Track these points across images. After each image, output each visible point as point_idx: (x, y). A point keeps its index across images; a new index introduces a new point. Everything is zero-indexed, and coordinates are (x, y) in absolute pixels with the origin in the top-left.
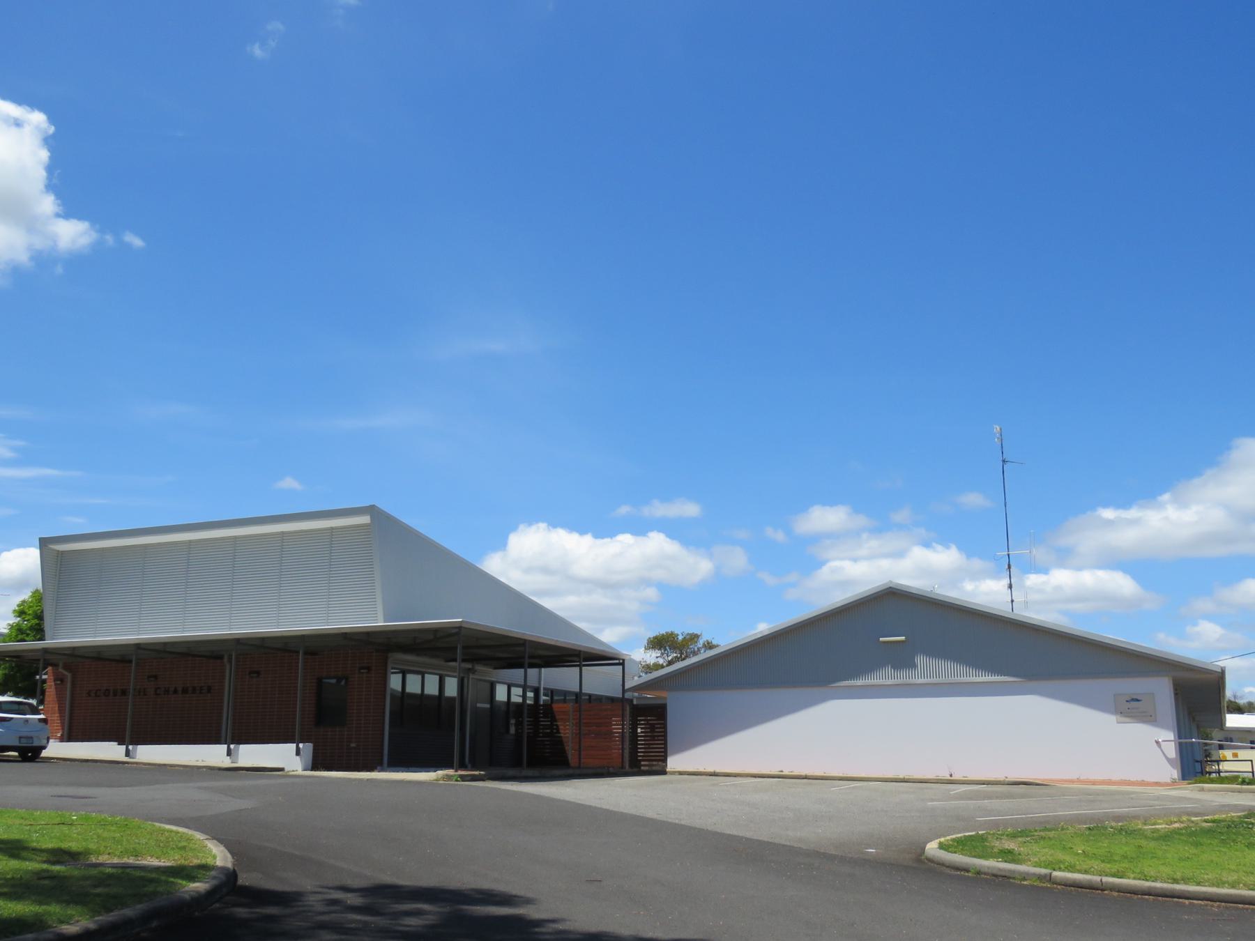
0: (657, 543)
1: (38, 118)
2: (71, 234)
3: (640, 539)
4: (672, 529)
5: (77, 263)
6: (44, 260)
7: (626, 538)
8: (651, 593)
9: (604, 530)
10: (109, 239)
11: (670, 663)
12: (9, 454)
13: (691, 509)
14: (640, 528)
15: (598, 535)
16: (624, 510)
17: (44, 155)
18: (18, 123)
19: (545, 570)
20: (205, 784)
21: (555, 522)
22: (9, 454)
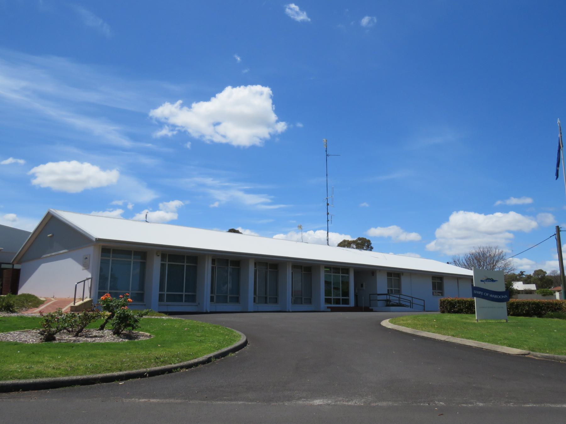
0: (513, 216)
1: (267, 90)
2: (281, 127)
3: (505, 214)
4: (518, 209)
5: (283, 135)
6: (273, 136)
7: (498, 214)
8: (511, 236)
9: (487, 210)
10: (292, 126)
11: (213, 187)
12: (269, 201)
13: (528, 201)
14: (505, 209)
15: (486, 214)
16: (499, 203)
17: (270, 101)
18: (262, 94)
19: (467, 229)
20: (93, 97)
21: (468, 209)
22: (269, 201)
